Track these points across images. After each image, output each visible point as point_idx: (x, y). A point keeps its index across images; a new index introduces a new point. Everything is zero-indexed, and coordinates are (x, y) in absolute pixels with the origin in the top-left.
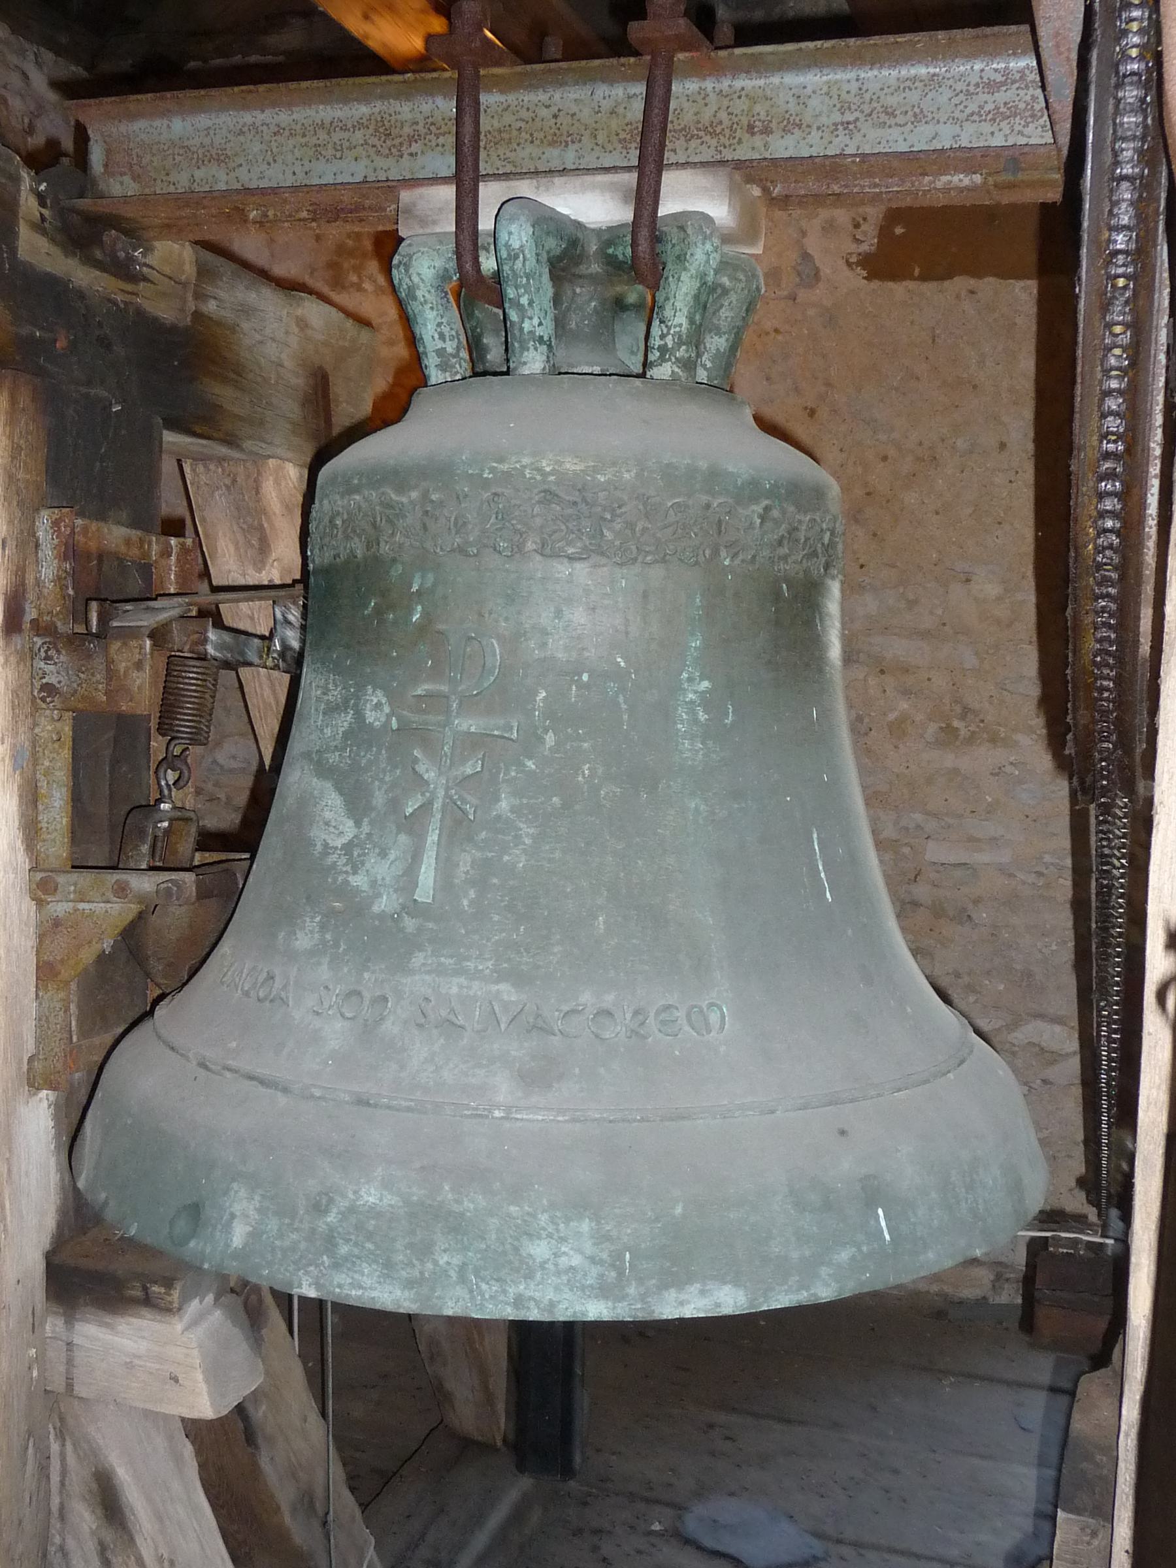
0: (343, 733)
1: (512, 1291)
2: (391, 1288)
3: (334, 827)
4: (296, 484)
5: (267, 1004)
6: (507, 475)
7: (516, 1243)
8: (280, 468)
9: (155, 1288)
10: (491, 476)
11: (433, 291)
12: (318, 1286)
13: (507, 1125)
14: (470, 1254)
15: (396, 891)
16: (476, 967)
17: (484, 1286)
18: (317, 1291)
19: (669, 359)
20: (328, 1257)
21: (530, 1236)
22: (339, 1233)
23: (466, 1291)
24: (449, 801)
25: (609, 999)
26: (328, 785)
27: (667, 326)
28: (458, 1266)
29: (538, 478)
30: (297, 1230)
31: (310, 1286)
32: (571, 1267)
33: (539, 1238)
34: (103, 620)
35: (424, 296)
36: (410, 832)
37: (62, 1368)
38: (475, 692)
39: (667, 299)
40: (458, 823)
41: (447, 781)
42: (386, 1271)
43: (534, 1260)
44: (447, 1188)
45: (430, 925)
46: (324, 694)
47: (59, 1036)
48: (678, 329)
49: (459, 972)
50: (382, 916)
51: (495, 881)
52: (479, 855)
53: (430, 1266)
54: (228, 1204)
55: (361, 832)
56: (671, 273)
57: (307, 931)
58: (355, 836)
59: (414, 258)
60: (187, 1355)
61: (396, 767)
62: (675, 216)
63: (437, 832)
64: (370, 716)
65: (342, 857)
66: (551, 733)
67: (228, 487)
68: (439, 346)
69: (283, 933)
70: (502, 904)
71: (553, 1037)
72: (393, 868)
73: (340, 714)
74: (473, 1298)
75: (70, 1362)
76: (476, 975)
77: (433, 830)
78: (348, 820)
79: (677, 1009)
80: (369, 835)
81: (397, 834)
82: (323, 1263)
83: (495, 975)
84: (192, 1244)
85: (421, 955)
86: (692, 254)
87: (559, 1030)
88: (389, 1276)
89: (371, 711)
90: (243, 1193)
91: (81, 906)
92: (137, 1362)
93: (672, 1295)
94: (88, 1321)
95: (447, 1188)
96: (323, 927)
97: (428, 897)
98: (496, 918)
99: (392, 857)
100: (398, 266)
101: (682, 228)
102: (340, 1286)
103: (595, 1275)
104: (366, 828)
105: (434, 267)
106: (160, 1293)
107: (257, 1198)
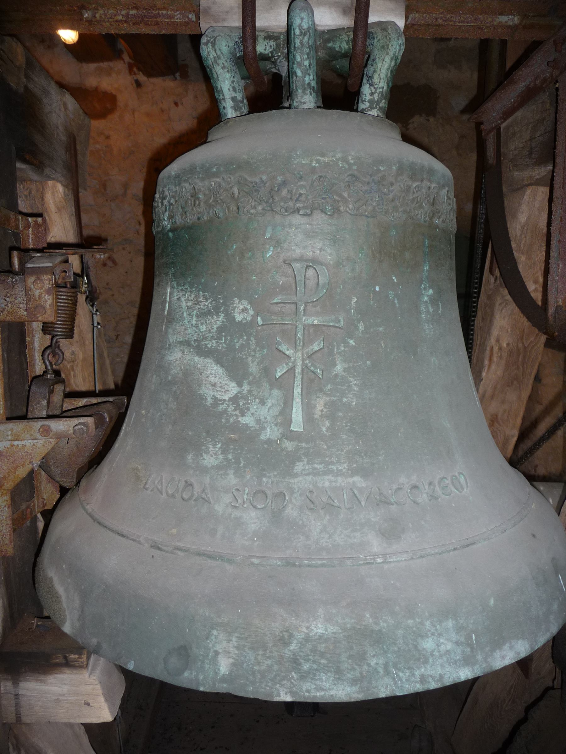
0: (217, 328)
1: (417, 673)
2: (343, 687)
3: (220, 387)
4: (63, 196)
5: (192, 502)
6: (327, 165)
7: (415, 643)
8: (54, 187)
9: (72, 656)
10: (317, 165)
11: (228, 61)
12: (292, 693)
13: (386, 567)
14: (389, 655)
15: (276, 425)
16: (337, 468)
17: (401, 674)
18: (293, 697)
19: (376, 108)
20: (295, 673)
21: (422, 637)
22: (300, 656)
23: (391, 680)
24: (305, 368)
25: (414, 479)
26: (210, 361)
27: (374, 88)
28: (383, 664)
29: (347, 166)
30: (269, 658)
31: (286, 694)
32: (448, 651)
33: (427, 637)
34: (22, 263)
35: (223, 64)
36: (280, 388)
37: (13, 709)
38: (315, 300)
39: (375, 72)
40: (312, 381)
41: (303, 355)
42: (338, 676)
43: (427, 651)
44: (368, 616)
45: (304, 445)
46: (195, 304)
47: (5, 522)
48: (381, 90)
49: (327, 472)
50: (269, 441)
51: (340, 414)
52: (327, 399)
53: (365, 667)
54: (211, 645)
55: (243, 390)
56: (378, 56)
57: (211, 453)
58: (238, 393)
59: (217, 39)
60: (94, 689)
61: (263, 348)
62: (379, 24)
63: (300, 387)
64: (239, 317)
65: (231, 406)
66: (361, 323)
67: (26, 197)
68: (233, 95)
69: (191, 456)
70: (347, 428)
71: (392, 506)
72: (271, 411)
73: (212, 317)
74: (395, 683)
75: (18, 705)
76: (339, 473)
77: (297, 386)
78: (231, 382)
79: (446, 478)
80: (250, 392)
81: (271, 390)
82: (293, 677)
83: (350, 472)
84: (186, 674)
85: (301, 464)
86: (392, 45)
87: (394, 501)
88: (340, 679)
89: (239, 313)
90: (222, 636)
91: (16, 443)
92: (61, 698)
93: (497, 654)
94: (27, 680)
95: (368, 616)
96: (225, 451)
97: (300, 428)
98: (344, 437)
99: (269, 403)
100: (206, 44)
101: (385, 30)
102: (308, 691)
103: (460, 653)
104: (246, 387)
105: (229, 47)
106: (75, 658)
107: (234, 639)
